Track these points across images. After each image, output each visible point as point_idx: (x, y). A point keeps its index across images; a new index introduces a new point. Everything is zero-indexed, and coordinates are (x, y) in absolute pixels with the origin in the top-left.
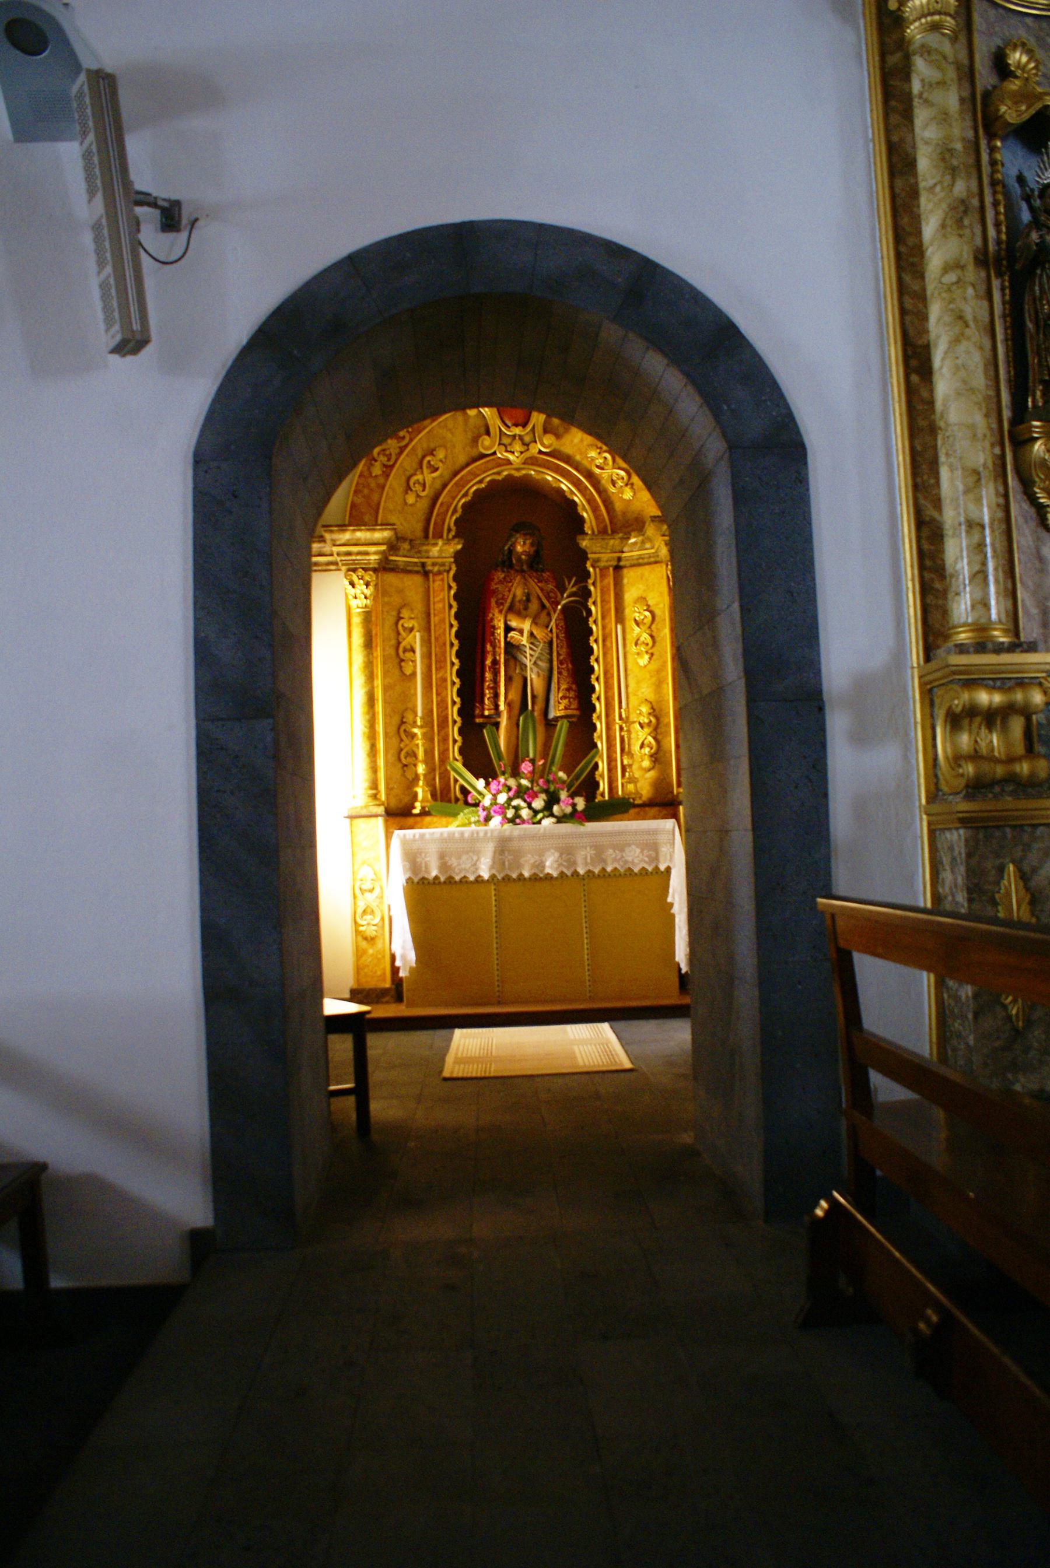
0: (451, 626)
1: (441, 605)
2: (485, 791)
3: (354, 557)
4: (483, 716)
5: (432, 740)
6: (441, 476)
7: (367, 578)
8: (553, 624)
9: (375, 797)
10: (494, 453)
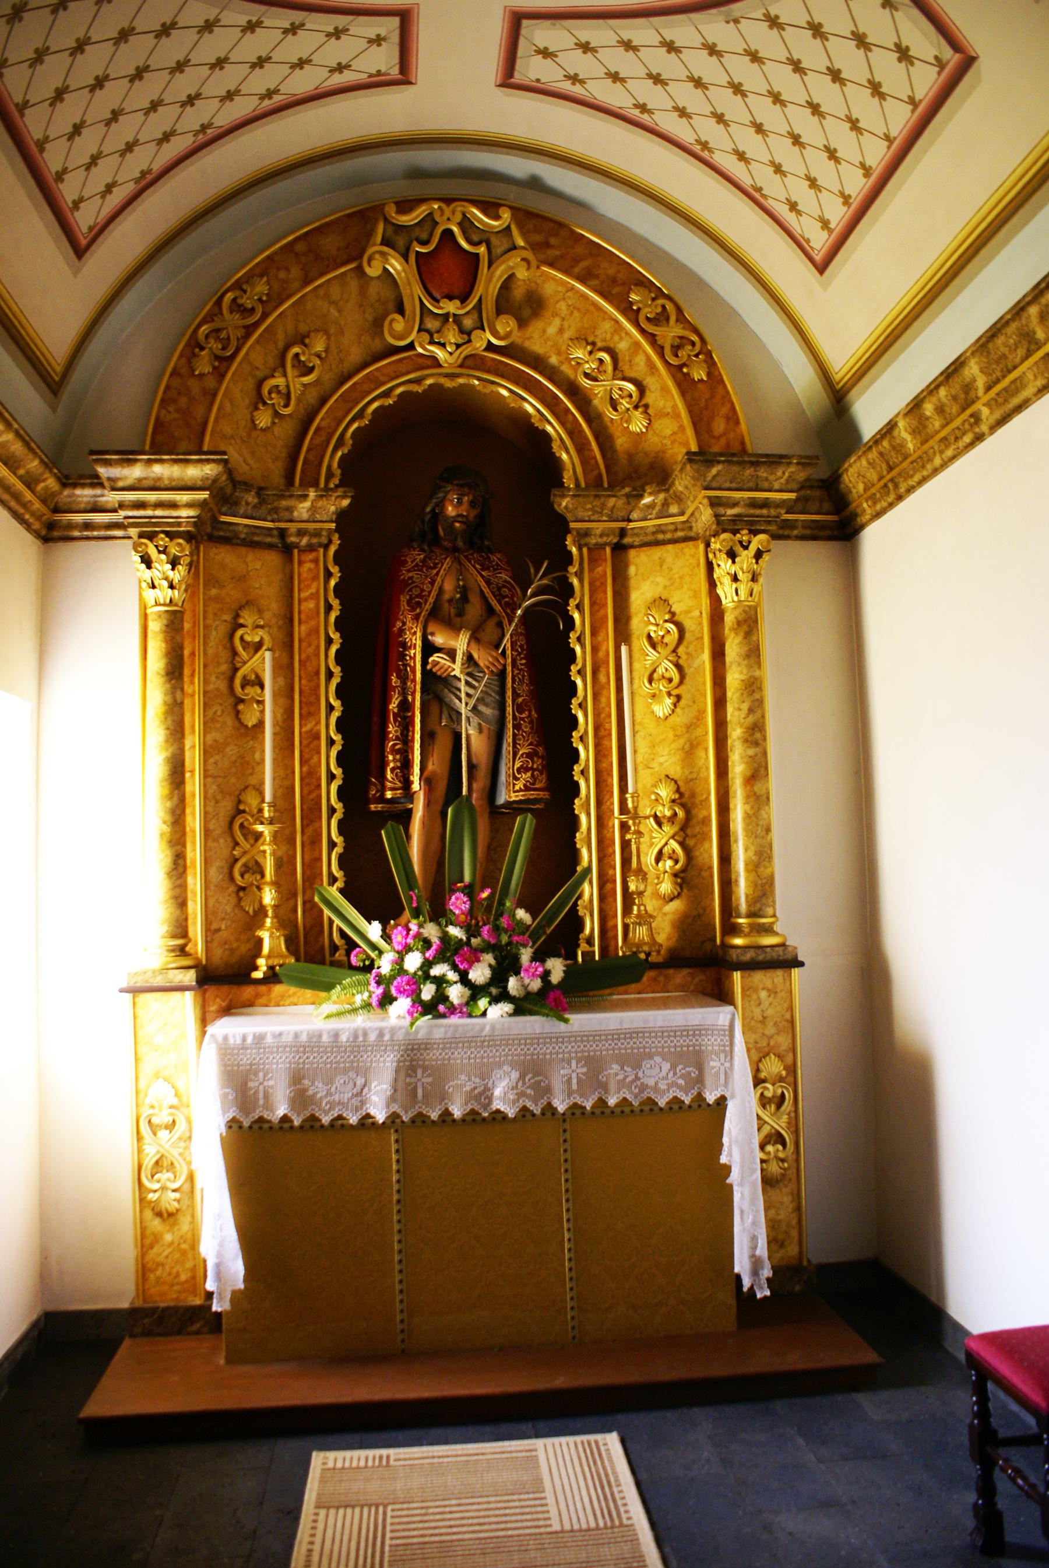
0: (329, 641)
1: (311, 605)
2: (382, 944)
3: (149, 512)
4: (382, 799)
5: (292, 841)
6: (317, 382)
7: (174, 550)
8: (506, 641)
9: (182, 951)
10: (411, 346)
